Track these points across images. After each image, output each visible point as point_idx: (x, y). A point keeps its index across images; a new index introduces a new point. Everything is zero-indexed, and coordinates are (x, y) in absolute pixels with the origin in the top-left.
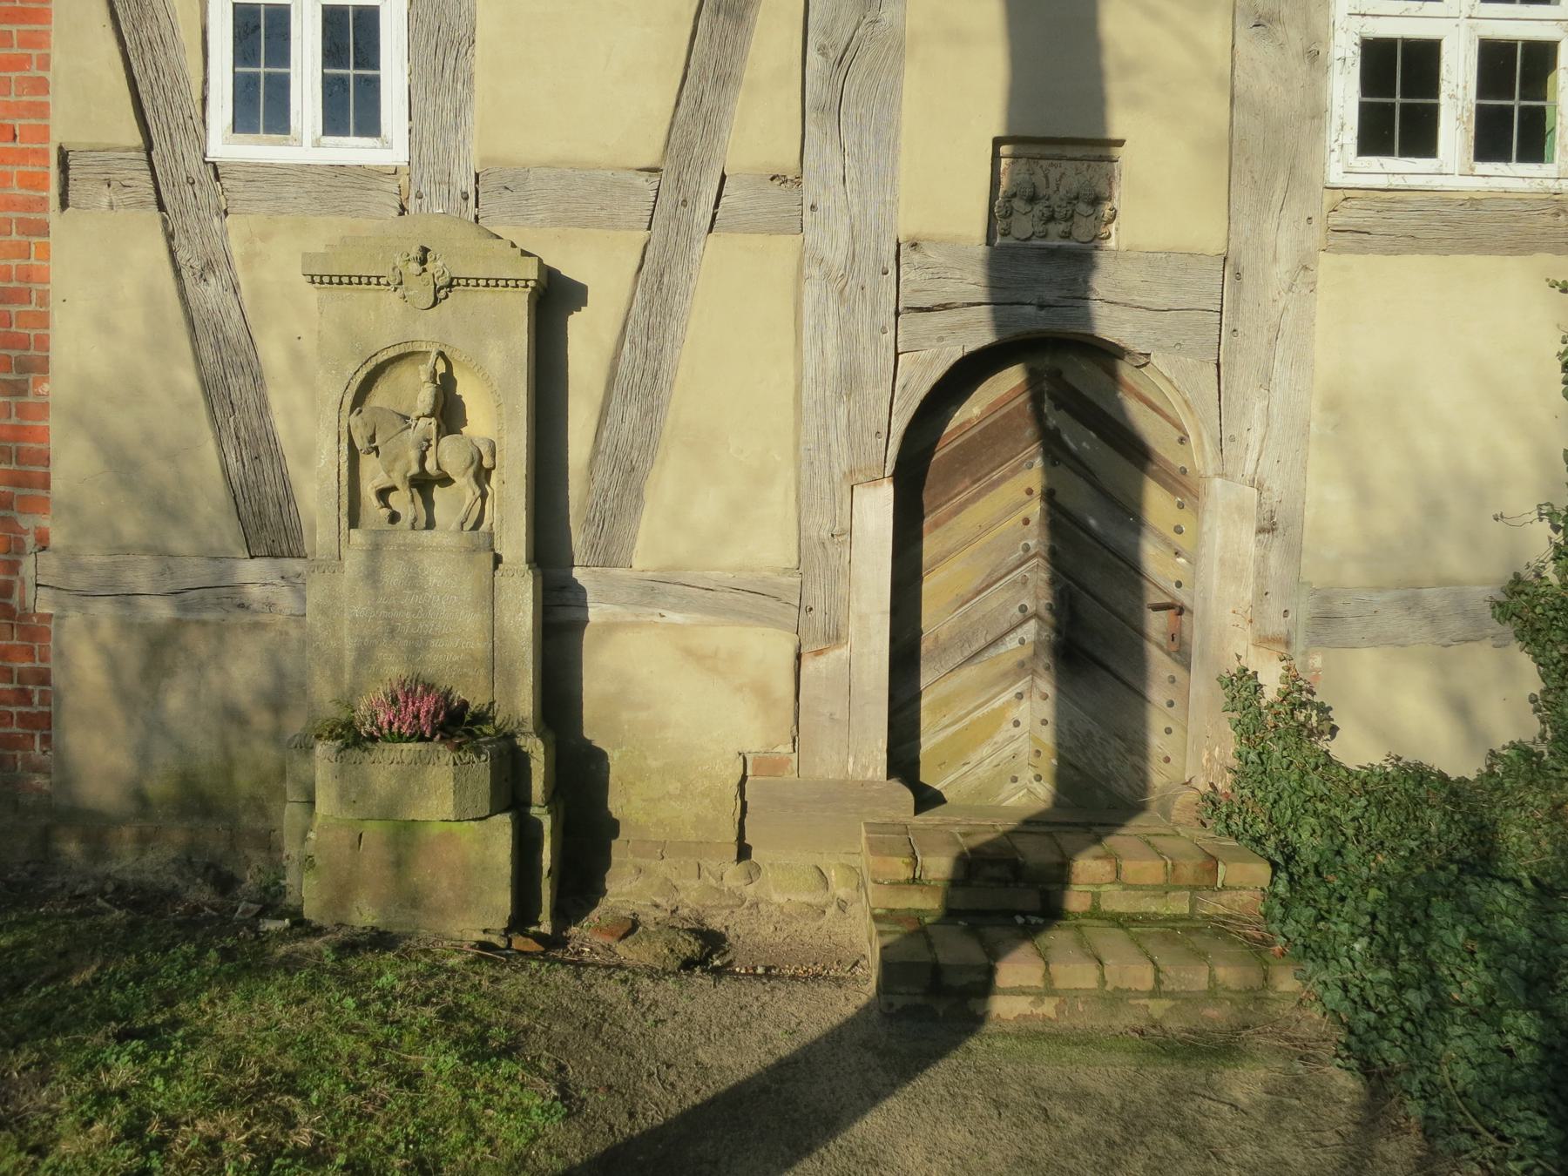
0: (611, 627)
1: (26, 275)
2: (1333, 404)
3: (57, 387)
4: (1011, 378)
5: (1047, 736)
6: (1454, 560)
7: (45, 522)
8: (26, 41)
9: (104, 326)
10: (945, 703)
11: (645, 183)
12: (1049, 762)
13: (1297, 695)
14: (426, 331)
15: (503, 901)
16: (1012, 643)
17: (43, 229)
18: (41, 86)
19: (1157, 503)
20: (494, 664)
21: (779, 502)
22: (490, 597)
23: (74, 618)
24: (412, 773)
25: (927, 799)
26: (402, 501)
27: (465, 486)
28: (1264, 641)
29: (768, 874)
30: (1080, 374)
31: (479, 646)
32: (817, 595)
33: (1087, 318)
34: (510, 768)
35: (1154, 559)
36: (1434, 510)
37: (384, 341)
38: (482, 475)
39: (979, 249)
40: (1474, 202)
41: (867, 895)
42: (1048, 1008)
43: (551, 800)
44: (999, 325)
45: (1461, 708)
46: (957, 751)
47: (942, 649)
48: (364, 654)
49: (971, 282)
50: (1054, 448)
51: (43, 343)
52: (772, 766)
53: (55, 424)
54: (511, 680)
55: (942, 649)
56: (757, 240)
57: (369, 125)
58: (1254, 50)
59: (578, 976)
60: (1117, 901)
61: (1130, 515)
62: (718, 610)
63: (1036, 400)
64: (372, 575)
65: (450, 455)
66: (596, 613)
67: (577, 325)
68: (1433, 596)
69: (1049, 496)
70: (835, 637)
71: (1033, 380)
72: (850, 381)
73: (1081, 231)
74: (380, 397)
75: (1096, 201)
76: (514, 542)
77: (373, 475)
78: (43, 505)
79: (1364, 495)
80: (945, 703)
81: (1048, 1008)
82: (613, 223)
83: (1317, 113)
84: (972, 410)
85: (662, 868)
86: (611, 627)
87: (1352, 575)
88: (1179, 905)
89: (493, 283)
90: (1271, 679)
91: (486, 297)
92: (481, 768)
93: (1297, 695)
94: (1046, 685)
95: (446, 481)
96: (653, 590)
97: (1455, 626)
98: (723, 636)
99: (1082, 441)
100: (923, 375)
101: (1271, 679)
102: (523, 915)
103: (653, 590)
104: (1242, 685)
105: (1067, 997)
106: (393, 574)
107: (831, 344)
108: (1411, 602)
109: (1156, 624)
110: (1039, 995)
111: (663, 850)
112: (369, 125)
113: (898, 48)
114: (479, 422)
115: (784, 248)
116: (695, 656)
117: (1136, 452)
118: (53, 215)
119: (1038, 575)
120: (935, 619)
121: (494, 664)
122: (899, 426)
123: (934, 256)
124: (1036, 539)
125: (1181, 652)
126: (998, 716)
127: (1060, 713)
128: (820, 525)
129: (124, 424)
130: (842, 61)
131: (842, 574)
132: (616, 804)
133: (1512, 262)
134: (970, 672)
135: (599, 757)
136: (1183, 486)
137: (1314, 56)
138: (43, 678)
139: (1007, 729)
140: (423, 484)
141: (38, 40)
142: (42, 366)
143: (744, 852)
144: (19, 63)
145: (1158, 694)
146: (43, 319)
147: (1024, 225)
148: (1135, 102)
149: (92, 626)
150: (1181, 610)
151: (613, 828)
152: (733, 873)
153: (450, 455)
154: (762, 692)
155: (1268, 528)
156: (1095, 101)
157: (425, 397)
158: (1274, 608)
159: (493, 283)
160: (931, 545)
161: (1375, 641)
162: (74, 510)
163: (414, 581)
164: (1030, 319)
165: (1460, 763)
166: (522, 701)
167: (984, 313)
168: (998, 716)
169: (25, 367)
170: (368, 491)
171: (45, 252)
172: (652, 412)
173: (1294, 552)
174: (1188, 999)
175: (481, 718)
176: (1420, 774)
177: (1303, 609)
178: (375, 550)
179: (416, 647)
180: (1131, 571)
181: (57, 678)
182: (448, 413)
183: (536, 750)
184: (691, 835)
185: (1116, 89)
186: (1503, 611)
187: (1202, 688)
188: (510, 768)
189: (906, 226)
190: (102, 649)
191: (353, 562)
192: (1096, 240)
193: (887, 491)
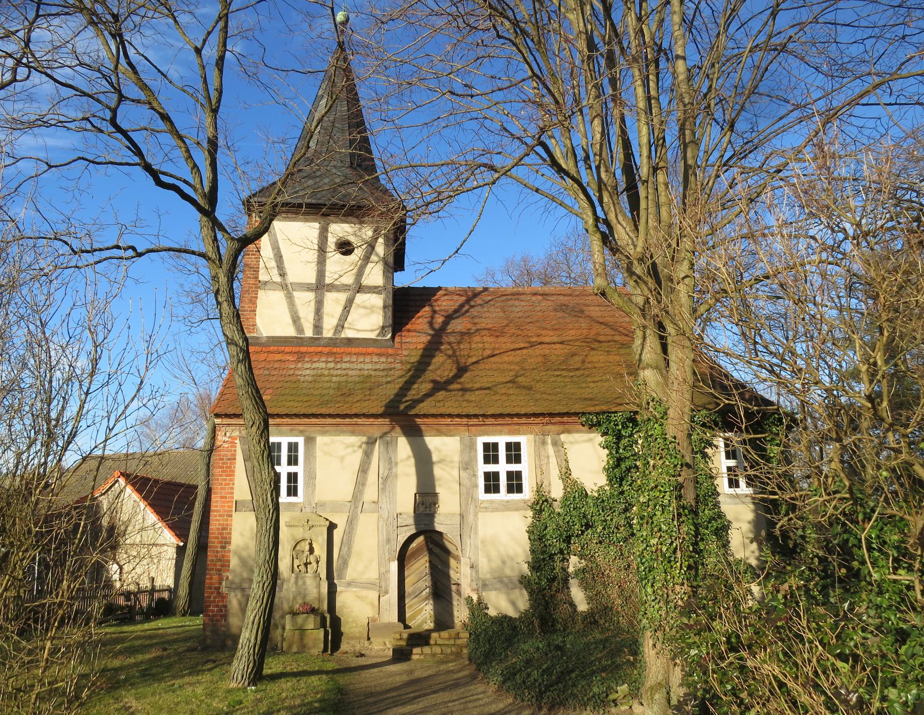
0: (341, 592)
1: (227, 525)
2: (483, 542)
3: (232, 547)
4: (421, 539)
5: (432, 613)
6: (508, 572)
7: (228, 574)
8: (231, 480)
9: (242, 535)
10: (411, 606)
11: (349, 504)
12: (433, 619)
13: (480, 602)
14: (307, 535)
15: (322, 646)
16: (424, 593)
17: (231, 516)
18: (233, 488)
19: (452, 562)
20: (319, 599)
21: (375, 565)
22: (319, 586)
23: (232, 594)
24: (305, 620)
25: (407, 627)
26: (302, 568)
27: (314, 564)
28: (473, 590)
29: (374, 643)
30: (435, 537)
31: (316, 596)
32: (383, 585)
33: (434, 527)
34: (323, 619)
35: (452, 573)
36: (504, 562)
37: (299, 537)
38: (318, 562)
39: (412, 514)
40: (508, 502)
41: (407, 694)
42: (422, 657)
43: (331, 626)
44: (417, 529)
45: (513, 603)
46: (413, 617)
47: (410, 595)
48: (294, 598)
49: (411, 521)
50: (430, 552)
51: (230, 538)
52: (374, 620)
53: (231, 554)
54: (323, 603)
55: (410, 595)
56: (370, 514)
57: (295, 494)
58: (464, 474)
59: (434, 381)
60: (440, 642)
61: (447, 565)
62: (363, 588)
63: (427, 542)
64: (296, 583)
65: (312, 559)
66: (339, 589)
67: (335, 531)
68: (505, 580)
69: (430, 562)
70: (387, 592)
71: (426, 539)
72: (388, 541)
73: (432, 510)
74: (298, 548)
75: (435, 504)
76: (323, 575)
77: (297, 562)
78: (228, 571)
79: (490, 560)
80: (411, 606)
81: (422, 657)
82: (342, 512)
83: (476, 486)
84: (414, 545)
85: (352, 642)
86: (341, 592)
87: (489, 576)
88: (452, 642)
89: (320, 526)
90: (475, 598)
91: (319, 528)
92: (318, 619)
93: (480, 602)
94: (431, 602)
95: (310, 563)
96: (349, 584)
97: (510, 586)
98: (364, 593)
99: (437, 550)
100: (402, 539)
101: (475, 598)
102: (325, 650)
103: (349, 584)
104: (469, 600)
105: (426, 654)
106: (300, 582)
107: (385, 533)
108: (501, 582)
109: (454, 588)
110: (420, 655)
111: (352, 638)
112: (295, 494)
113: (396, 476)
114: (316, 552)
115: (376, 515)
116: (359, 597)
117: (447, 552)
118: (234, 513)
119: (428, 578)
120: (408, 589)
121: (319, 599)
122: (398, 550)
123: (404, 516)
124: (427, 571)
125: (459, 593)
126: (422, 609)
127: (435, 607)
128: (383, 570)
129: (244, 554)
130: (386, 479)
131: (387, 580)
132: (343, 629)
133: (516, 513)
134: (416, 599)
135: (339, 619)
136: (457, 559)
137: (475, 475)
138: (225, 606)
139: (424, 612)
140: (306, 564)
141: (232, 480)
142: (230, 543)
143: (369, 639)
144: (229, 484)
145: (455, 603)
146: (230, 534)
147: (421, 509)
148: (440, 485)
149: (236, 595)
150: (459, 585)
151: (342, 634)
152: (366, 643)
153: (312, 559)
154: (372, 604)
155: (472, 567)
156: (434, 487)
157: (307, 548)
158: (474, 583)
159: (320, 526)
160: (406, 573)
161: (495, 589)
162: (234, 571)
163: (304, 583)
164: (423, 527)
165: (512, 613)
166: (325, 607)
167: (413, 527)
168: (422, 609)
169: (226, 543)
170: (295, 566)
171: (231, 520)
172: (350, 548)
173: (477, 572)
174: (447, 654)
175: (318, 609)
176: (505, 617)
177: (480, 584)
178: (297, 578)
179: (305, 596)
180: (448, 577)
181: (229, 607)
182: (311, 550)
183: (328, 616)
184: (358, 635)
185: (437, 483)
186: (521, 583)
187: (463, 601)
188: (323, 619)
189: (398, 511)
190: (238, 600)
191: (293, 580)
192: (435, 512)
193: (396, 563)
